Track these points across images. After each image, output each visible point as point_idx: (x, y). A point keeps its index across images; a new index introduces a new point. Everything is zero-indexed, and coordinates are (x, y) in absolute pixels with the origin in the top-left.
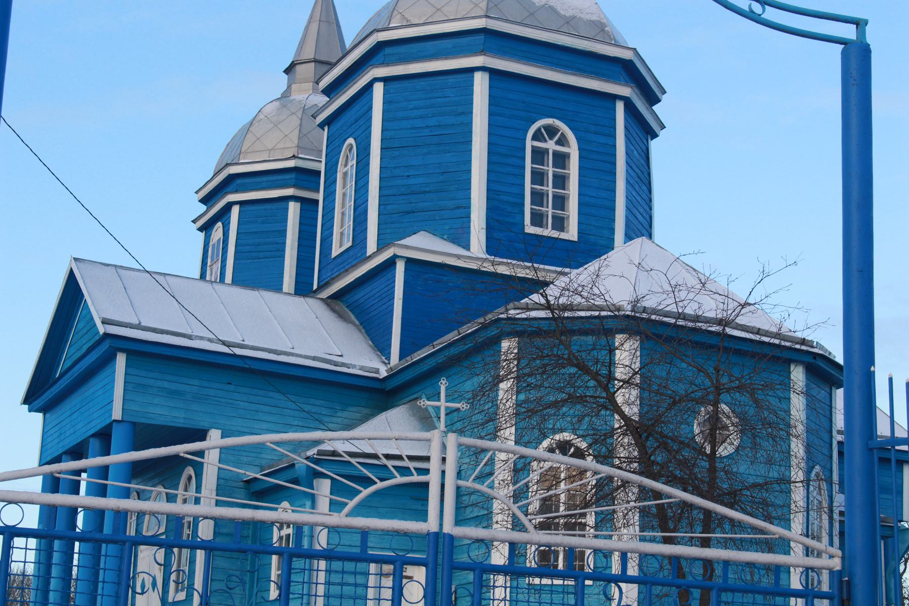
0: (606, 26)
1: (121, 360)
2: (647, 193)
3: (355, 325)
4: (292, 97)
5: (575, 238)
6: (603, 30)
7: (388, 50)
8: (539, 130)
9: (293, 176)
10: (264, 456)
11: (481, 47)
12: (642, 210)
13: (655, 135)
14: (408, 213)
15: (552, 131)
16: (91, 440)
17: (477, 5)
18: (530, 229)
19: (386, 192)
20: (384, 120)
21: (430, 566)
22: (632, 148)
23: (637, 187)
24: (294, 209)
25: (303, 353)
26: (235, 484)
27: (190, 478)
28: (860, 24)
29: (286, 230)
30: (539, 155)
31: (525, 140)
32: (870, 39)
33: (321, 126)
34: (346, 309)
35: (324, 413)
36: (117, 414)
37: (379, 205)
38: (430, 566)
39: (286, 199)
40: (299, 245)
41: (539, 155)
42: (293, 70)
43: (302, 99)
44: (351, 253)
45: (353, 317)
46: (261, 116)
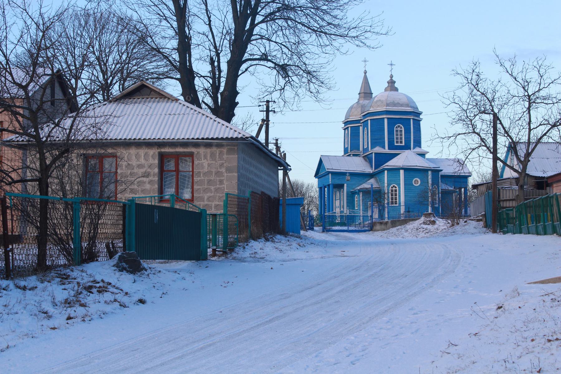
1: (330, 175)
18: (396, 144)
30: (397, 131)
36: (330, 183)
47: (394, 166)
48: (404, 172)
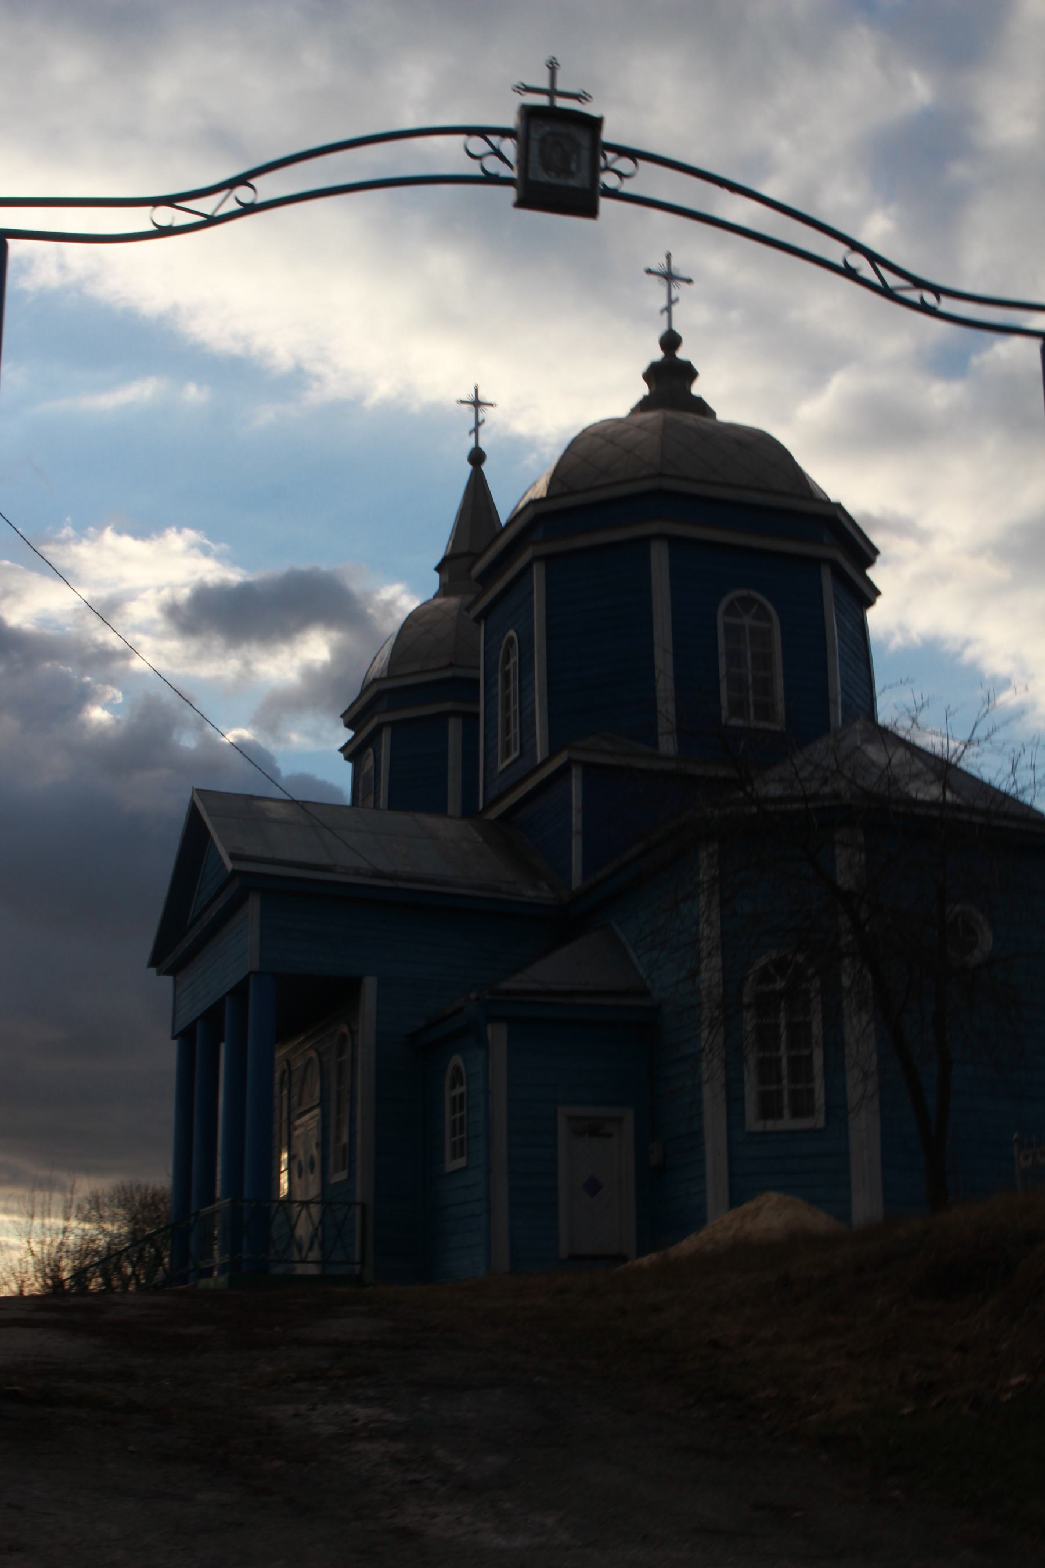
24: (454, 728)
33: (477, 619)
39: (445, 715)
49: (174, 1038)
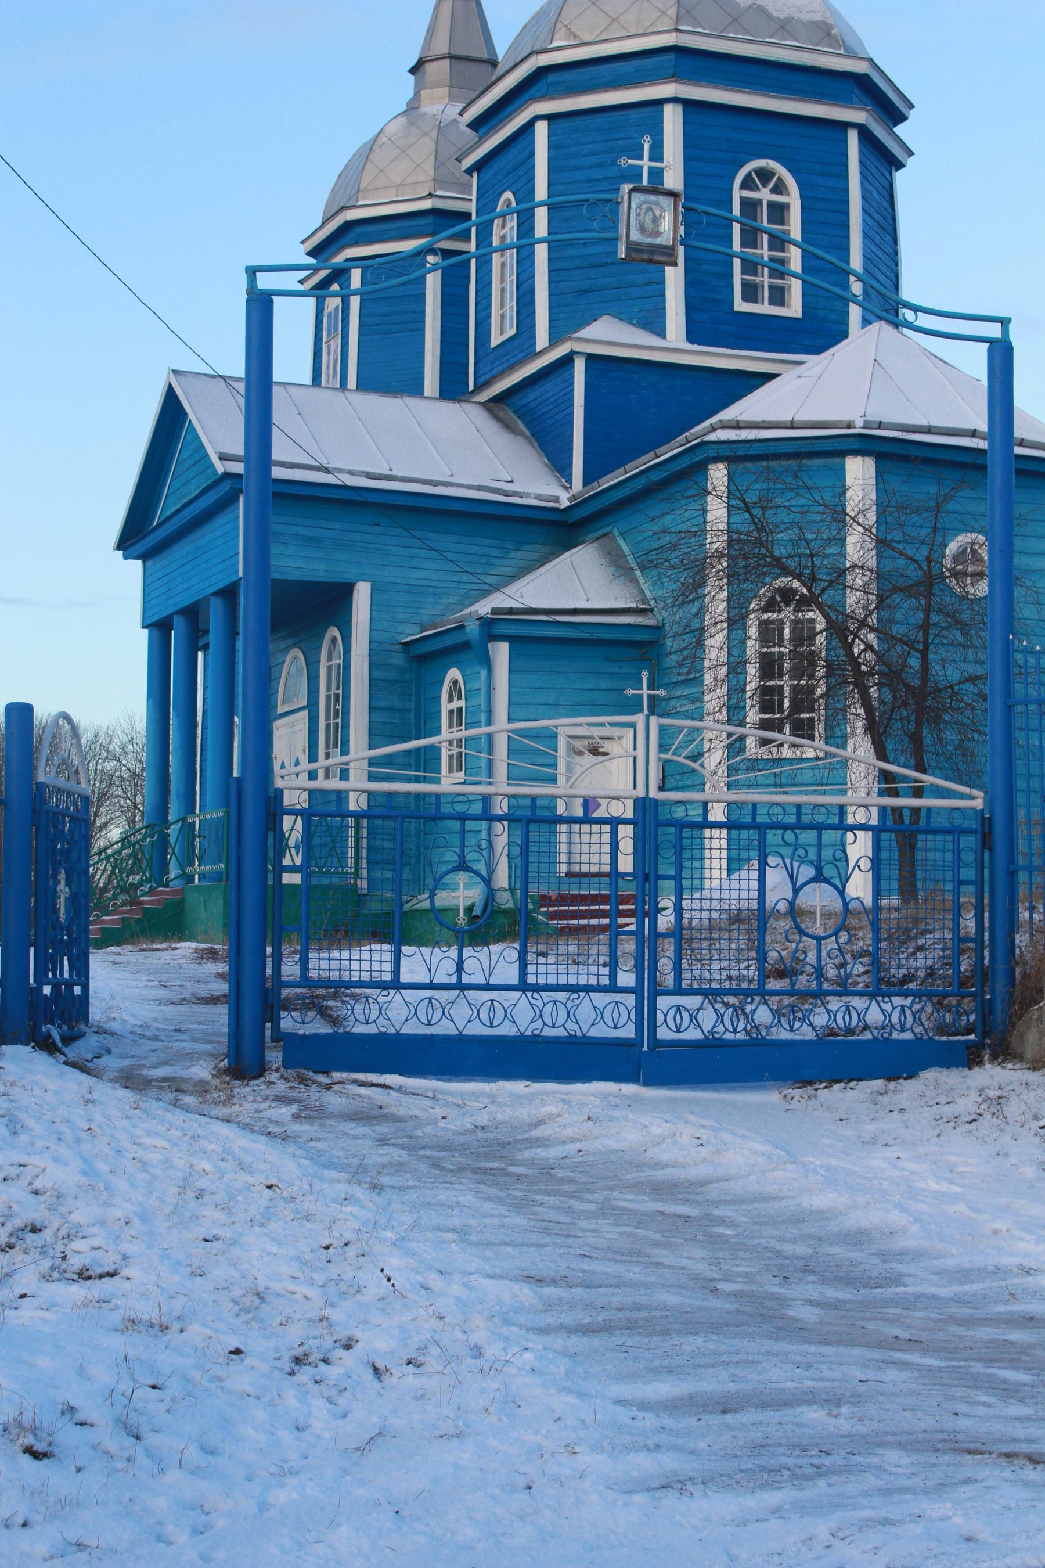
0: (833, 28)
2: (891, 243)
3: (525, 437)
4: (423, 110)
5: (799, 314)
6: (829, 34)
7: (552, 78)
8: (749, 175)
9: (429, 220)
10: (423, 611)
11: (672, 70)
12: (884, 269)
13: (900, 165)
14: (587, 291)
15: (765, 176)
16: (212, 598)
17: (664, 13)
18: (740, 305)
19: (558, 265)
20: (551, 171)
21: (640, 825)
22: (870, 188)
23: (877, 239)
25: (465, 482)
26: (391, 648)
27: (334, 640)
28: (1004, 322)
29: (425, 294)
31: (731, 190)
32: (1013, 338)
33: (469, 171)
34: (513, 415)
35: (493, 554)
37: (549, 283)
38: (640, 825)
40: (442, 314)
41: (750, 207)
42: (421, 69)
43: (436, 112)
44: (516, 343)
45: (522, 426)
46: (383, 139)
47: (792, 426)
48: (879, 474)
49: (143, 627)
